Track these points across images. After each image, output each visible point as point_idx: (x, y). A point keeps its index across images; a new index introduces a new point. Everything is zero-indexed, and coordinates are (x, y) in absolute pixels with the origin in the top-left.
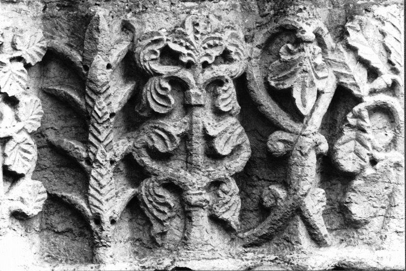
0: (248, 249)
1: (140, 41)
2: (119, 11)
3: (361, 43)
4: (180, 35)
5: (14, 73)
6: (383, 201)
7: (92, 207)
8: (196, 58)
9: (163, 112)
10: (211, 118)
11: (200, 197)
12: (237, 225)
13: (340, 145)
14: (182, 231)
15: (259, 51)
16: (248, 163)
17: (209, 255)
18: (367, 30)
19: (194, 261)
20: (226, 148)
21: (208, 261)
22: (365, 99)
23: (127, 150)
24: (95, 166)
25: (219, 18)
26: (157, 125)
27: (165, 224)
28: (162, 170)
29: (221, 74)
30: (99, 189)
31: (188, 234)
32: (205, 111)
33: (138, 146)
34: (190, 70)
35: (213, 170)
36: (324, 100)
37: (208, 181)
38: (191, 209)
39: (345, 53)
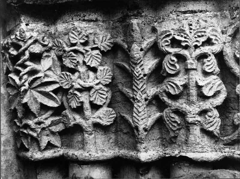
0: (227, 146)
1: (160, 36)
2: (149, 21)
4: (181, 31)
5: (94, 55)
7: (135, 122)
8: (190, 43)
9: (173, 73)
10: (202, 76)
11: (194, 119)
12: (218, 134)
14: (185, 136)
15: (230, 38)
16: (225, 100)
17: (200, 150)
19: (191, 153)
20: (210, 92)
21: (199, 153)
23: (155, 93)
24: (136, 102)
25: (206, 21)
26: (170, 80)
27: (176, 132)
28: (173, 104)
29: (206, 52)
30: (138, 114)
31: (188, 138)
32: (197, 72)
33: (161, 91)
34: (188, 50)
35: (202, 104)
37: (199, 110)
38: (189, 125)
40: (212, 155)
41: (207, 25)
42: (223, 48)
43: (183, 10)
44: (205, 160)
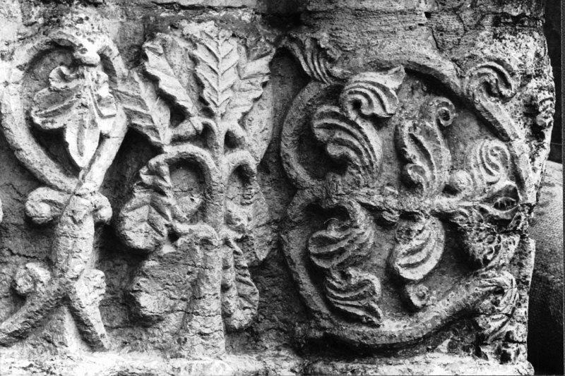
6: (184, 291)
13: (128, 211)
18: (172, 53)
22: (166, 149)
39: (141, 84)
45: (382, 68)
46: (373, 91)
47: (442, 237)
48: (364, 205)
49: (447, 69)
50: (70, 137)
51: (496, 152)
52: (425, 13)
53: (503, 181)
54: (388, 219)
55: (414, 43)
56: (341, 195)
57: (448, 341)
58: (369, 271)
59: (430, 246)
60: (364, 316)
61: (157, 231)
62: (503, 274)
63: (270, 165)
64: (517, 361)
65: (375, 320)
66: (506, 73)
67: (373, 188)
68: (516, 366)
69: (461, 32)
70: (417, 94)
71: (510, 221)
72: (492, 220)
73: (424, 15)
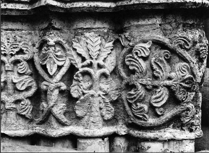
3: (79, 47)
6: (88, 110)
10: (17, 76)
11: (10, 106)
13: (72, 87)
15: (38, 50)
17: (14, 128)
18: (81, 42)
20: (23, 87)
22: (80, 69)
25: (21, 37)
29: (19, 59)
36: (63, 70)
37: (14, 100)
39: (73, 51)
40: (23, 132)
41: (22, 39)
42: (33, 56)
43: (5, 28)
44: (17, 135)
45: (145, 42)
46: (141, 49)
47: (168, 93)
48: (141, 84)
49: (167, 41)
50: (48, 67)
51: (184, 66)
52: (159, 24)
53: (188, 75)
54: (148, 88)
55: (155, 34)
56: (133, 81)
57: (172, 125)
58: (145, 104)
59: (163, 96)
60: (142, 117)
61: (79, 92)
62: (189, 104)
63: (117, 73)
64: (196, 131)
65: (145, 119)
66: (187, 41)
67: (144, 79)
68: (195, 133)
69: (172, 30)
70: (157, 50)
71: (191, 88)
72: (184, 87)
73: (158, 25)
